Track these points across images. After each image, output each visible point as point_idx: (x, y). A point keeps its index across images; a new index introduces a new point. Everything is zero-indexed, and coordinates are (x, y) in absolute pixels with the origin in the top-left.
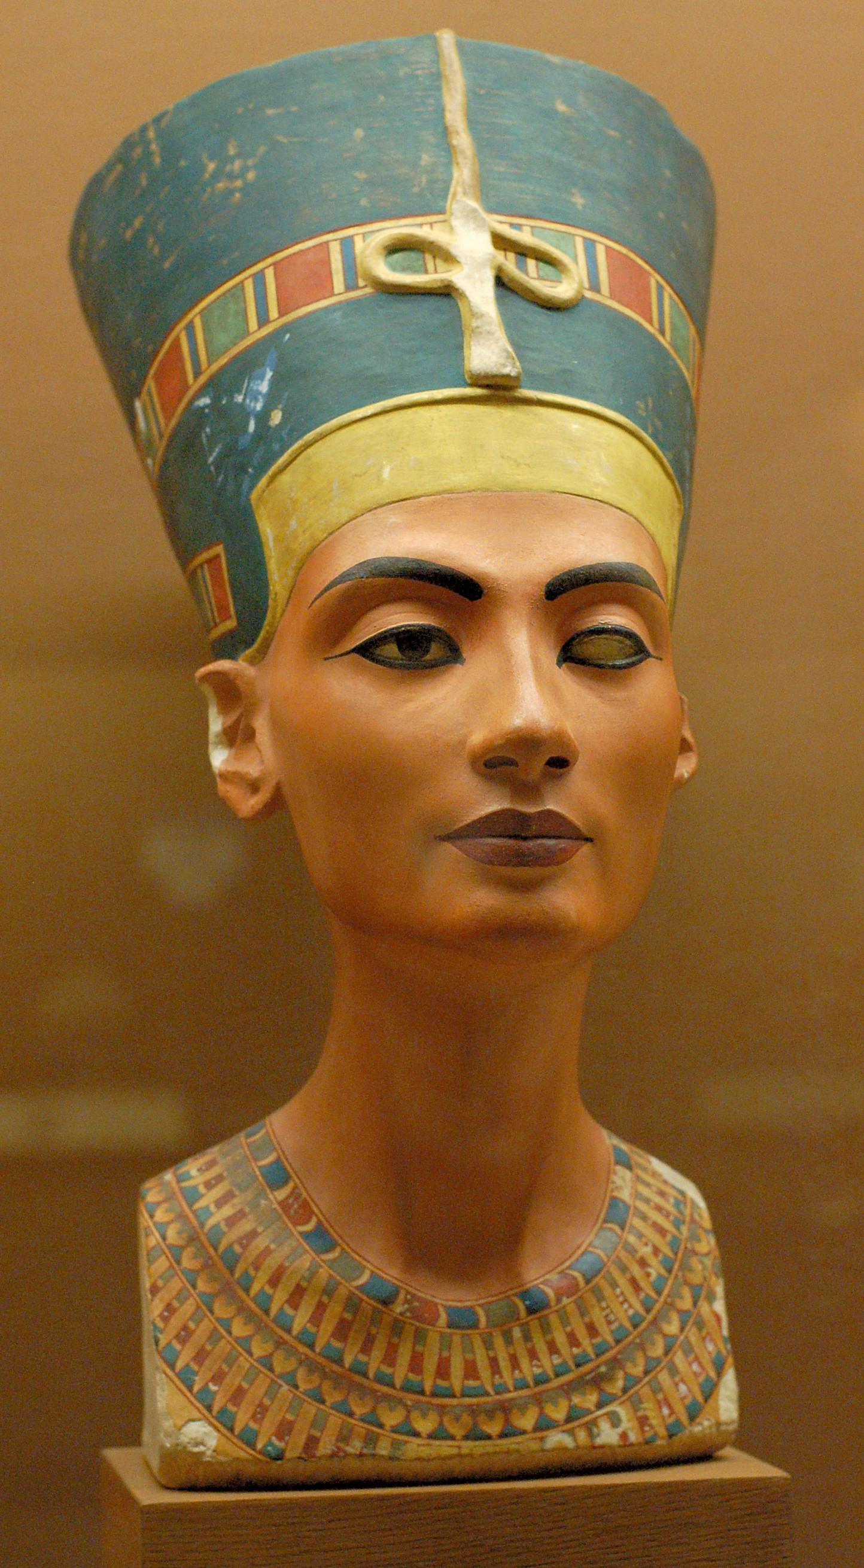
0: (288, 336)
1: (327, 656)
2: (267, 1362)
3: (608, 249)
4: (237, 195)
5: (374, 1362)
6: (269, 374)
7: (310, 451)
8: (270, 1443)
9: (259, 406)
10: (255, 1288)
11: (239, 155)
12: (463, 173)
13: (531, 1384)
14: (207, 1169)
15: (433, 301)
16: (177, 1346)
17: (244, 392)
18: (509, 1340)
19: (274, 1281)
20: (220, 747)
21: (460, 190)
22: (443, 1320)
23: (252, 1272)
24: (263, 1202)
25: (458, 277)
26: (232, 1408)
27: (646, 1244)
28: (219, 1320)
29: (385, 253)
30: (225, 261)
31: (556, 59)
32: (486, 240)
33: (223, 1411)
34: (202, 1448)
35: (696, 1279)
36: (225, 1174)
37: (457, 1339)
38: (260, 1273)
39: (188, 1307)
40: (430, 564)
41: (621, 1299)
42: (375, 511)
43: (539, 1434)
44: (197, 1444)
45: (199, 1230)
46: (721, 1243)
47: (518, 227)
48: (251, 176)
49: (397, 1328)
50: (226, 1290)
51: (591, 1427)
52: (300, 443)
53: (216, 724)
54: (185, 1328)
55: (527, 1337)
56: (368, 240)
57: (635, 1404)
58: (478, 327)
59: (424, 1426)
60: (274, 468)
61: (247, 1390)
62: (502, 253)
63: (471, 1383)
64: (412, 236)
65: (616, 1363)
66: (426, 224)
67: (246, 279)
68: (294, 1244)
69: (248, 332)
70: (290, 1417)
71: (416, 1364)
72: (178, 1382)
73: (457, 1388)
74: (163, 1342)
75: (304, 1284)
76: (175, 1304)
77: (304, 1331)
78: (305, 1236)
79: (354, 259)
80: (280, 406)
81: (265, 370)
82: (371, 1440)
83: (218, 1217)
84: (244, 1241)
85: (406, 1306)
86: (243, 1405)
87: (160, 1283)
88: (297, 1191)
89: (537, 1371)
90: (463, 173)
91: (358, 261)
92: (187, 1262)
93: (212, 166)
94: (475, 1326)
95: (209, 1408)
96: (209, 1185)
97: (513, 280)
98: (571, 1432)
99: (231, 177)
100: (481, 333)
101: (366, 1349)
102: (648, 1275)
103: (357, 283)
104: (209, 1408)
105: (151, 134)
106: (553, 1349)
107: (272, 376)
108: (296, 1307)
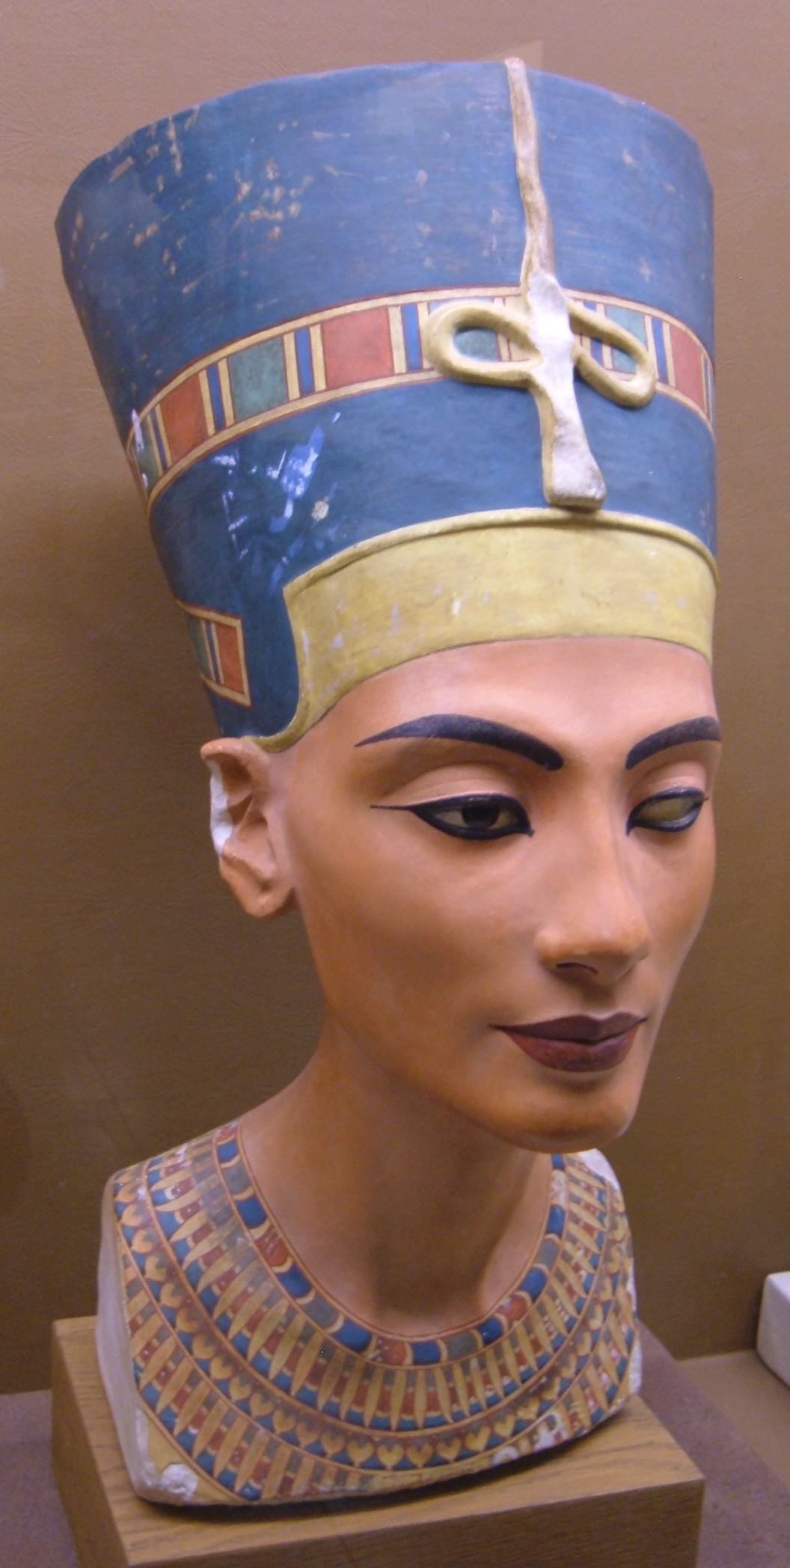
0: (338, 416)
1: (375, 804)
2: (244, 1405)
3: (672, 327)
4: (277, 230)
5: (346, 1403)
6: (313, 457)
7: (364, 562)
8: (247, 1485)
9: (300, 491)
10: (234, 1331)
11: (279, 181)
12: (537, 240)
13: (485, 1407)
14: (182, 1193)
15: (507, 397)
16: (158, 1387)
17: (280, 468)
18: (466, 1368)
19: (253, 1325)
20: (223, 823)
21: (536, 260)
22: (409, 1359)
23: (230, 1315)
24: (240, 1240)
25: (541, 378)
26: (211, 1452)
27: (579, 1249)
28: (198, 1361)
29: (454, 330)
30: (260, 306)
31: (620, 100)
32: (564, 323)
33: (204, 1453)
34: (182, 1490)
35: (614, 1267)
36: (201, 1203)
37: (421, 1374)
38: (238, 1317)
39: (168, 1347)
40: (508, 729)
41: (559, 1309)
42: (441, 653)
43: (489, 1453)
44: (178, 1486)
45: (177, 1266)
46: (632, 1225)
47: (591, 305)
48: (294, 209)
49: (368, 1372)
50: (206, 1333)
51: (532, 1436)
52: (348, 551)
53: (219, 800)
54: (165, 1368)
55: (483, 1365)
56: (435, 312)
57: (568, 1403)
58: (561, 437)
59: (389, 1459)
60: (315, 570)
61: (226, 1433)
62: (578, 338)
63: (433, 1414)
64: (485, 313)
65: (553, 1373)
66: (498, 297)
67: (286, 333)
68: (271, 1286)
69: (288, 399)
70: (266, 1460)
71: (384, 1404)
72: (160, 1425)
73: (420, 1422)
74: (143, 1383)
75: (281, 1330)
76: (155, 1343)
77: (280, 1375)
78: (281, 1277)
79: (418, 332)
80: (327, 499)
81: (309, 449)
82: (341, 1477)
83: (197, 1252)
84: (223, 1283)
85: (378, 1352)
86: (223, 1449)
87: (140, 1320)
88: (273, 1230)
89: (489, 1394)
90: (537, 240)
91: (424, 337)
92: (168, 1298)
93: (246, 188)
94: (437, 1359)
95: (189, 1451)
96: (187, 1214)
97: (591, 374)
98: (515, 1445)
99: (269, 206)
100: (563, 444)
101: (339, 1390)
102: (580, 1277)
103: (422, 364)
104: (189, 1451)
105: (172, 134)
106: (504, 1371)
107: (318, 459)
108: (272, 1351)
